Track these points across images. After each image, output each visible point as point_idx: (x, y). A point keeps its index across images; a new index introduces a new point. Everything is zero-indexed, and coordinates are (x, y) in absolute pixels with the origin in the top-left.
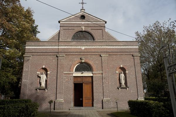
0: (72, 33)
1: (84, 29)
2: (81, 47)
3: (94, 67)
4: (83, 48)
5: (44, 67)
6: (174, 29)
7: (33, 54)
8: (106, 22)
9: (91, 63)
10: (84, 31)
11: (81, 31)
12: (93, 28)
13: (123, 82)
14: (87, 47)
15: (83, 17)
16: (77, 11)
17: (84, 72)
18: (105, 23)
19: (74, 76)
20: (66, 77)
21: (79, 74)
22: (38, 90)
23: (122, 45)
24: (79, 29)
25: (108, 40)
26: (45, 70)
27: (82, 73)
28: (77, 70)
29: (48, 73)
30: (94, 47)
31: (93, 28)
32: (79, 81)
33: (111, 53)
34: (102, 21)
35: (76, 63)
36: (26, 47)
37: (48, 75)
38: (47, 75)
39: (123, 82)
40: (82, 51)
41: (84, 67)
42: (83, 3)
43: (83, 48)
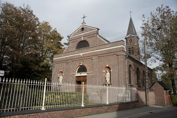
0: (76, 44)
1: (82, 39)
2: (79, 54)
3: (88, 68)
4: (81, 54)
5: (107, 66)
6: (148, 23)
7: (57, 63)
8: (98, 29)
9: (86, 65)
10: (84, 41)
11: (81, 41)
12: (89, 37)
13: (108, 80)
14: (84, 53)
15: (83, 29)
16: (79, 26)
17: (82, 73)
18: (97, 30)
19: (76, 76)
20: (71, 77)
21: (79, 75)
22: (104, 85)
23: (109, 46)
24: (79, 40)
25: (99, 44)
26: (108, 68)
27: (81, 74)
28: (79, 71)
29: (111, 71)
30: (88, 52)
31: (89, 37)
32: (79, 80)
33: (99, 56)
34: (95, 29)
35: (77, 66)
36: (54, 59)
37: (111, 73)
38: (62, 75)
39: (108, 80)
40: (81, 57)
41: (82, 69)
42: (84, 17)
43: (81, 54)
